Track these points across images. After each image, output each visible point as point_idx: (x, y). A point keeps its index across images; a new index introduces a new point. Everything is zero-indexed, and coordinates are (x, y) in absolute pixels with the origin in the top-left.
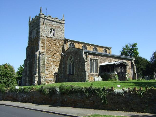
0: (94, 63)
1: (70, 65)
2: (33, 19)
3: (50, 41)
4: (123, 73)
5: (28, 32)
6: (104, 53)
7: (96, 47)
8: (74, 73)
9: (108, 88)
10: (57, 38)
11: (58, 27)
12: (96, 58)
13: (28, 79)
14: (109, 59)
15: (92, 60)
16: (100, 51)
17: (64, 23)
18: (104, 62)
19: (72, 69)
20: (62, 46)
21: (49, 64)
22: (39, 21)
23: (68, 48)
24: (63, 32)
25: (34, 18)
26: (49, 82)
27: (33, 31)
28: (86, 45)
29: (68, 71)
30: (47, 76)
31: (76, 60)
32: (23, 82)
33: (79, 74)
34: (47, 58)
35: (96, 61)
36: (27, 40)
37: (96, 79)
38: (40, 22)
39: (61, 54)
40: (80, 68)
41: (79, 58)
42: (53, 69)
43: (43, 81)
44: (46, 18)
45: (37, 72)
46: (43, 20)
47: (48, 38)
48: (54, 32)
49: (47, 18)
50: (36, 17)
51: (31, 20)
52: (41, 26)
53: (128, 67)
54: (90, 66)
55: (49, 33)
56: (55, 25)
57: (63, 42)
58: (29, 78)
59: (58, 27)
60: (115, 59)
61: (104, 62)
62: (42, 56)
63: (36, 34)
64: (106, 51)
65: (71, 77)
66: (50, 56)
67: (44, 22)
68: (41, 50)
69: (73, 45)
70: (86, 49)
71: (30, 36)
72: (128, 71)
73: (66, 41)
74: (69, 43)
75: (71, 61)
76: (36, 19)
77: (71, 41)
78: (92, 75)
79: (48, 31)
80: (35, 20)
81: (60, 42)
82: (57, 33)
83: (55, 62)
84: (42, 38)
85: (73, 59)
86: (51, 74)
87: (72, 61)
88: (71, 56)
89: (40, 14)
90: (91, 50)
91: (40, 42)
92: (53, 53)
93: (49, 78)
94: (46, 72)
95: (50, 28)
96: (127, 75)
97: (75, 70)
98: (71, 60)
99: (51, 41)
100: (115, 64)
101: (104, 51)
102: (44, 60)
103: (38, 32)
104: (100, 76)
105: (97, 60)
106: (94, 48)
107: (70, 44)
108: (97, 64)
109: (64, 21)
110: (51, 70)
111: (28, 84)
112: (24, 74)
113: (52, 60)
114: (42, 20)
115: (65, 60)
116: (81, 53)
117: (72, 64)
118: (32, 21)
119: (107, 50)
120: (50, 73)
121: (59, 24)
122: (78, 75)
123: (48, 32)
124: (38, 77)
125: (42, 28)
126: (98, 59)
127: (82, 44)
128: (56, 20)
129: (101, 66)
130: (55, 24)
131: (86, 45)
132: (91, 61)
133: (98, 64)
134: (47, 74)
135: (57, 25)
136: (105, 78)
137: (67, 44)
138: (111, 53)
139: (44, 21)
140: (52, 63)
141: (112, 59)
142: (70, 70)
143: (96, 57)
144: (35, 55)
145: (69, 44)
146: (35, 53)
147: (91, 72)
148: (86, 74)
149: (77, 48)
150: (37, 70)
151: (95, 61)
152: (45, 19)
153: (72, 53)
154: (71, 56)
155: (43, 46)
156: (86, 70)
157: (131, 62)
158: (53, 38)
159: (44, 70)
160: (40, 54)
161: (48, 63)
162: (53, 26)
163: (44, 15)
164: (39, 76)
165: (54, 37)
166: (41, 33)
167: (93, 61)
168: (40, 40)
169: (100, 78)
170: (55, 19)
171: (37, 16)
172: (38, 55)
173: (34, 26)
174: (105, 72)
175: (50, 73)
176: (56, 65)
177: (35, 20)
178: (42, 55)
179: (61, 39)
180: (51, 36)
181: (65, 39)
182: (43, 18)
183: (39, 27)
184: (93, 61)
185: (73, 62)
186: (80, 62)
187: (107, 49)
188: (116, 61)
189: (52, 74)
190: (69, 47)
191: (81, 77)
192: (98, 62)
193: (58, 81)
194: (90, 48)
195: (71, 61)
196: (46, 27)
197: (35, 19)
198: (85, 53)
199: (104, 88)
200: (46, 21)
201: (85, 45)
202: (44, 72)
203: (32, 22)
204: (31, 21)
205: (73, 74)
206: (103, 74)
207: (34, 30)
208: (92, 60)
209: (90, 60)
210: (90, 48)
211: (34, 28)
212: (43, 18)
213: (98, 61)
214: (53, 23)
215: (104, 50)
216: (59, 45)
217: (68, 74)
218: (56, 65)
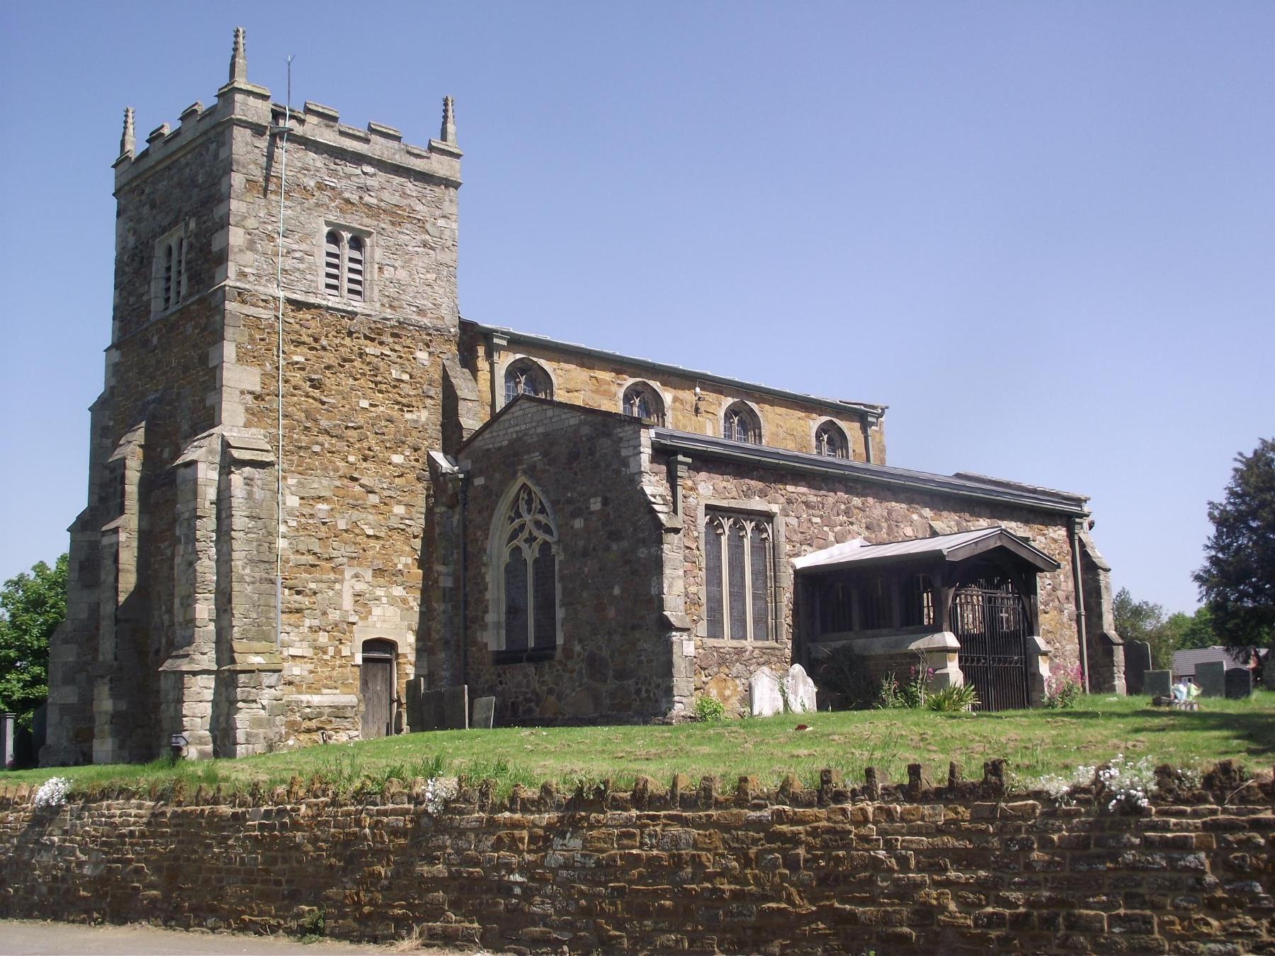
0: (747, 543)
1: (514, 569)
2: (155, 137)
3: (324, 342)
4: (1014, 635)
5: (114, 254)
6: (826, 456)
7: (746, 401)
8: (560, 641)
9: (952, 773)
10: (388, 313)
11: (397, 216)
12: (757, 504)
13: (105, 704)
14: (877, 509)
15: (727, 524)
16: (786, 434)
17: (457, 177)
18: (831, 537)
19: (537, 607)
20: (436, 392)
21: (310, 559)
22: (216, 155)
23: (493, 405)
24: (446, 257)
25: (167, 131)
26: (314, 724)
27: (159, 252)
28: (656, 385)
29: (497, 625)
30: (296, 670)
31: (574, 515)
32: (55, 735)
33: (605, 653)
34: (293, 501)
35: (758, 529)
36: (102, 331)
37: (766, 701)
38: (228, 167)
39: (432, 462)
40: (617, 591)
41: (605, 503)
42: (348, 603)
43: (257, 722)
44: (290, 124)
45: (206, 629)
46: (263, 143)
47: (305, 315)
48: (356, 255)
49: (298, 130)
50: (188, 115)
51: (135, 147)
52: (234, 205)
53: (1043, 582)
54: (703, 574)
55: (312, 269)
56: (367, 199)
57: (451, 352)
58: (115, 695)
59: (397, 216)
60: (927, 512)
61: (831, 537)
62: (249, 481)
63: (184, 279)
64: (835, 438)
65: (524, 677)
66: (321, 485)
67: (268, 167)
68: (234, 423)
69: (541, 380)
70: (661, 413)
71: (130, 294)
72: (1045, 621)
73: (473, 340)
74: (505, 360)
75: (522, 527)
76: (188, 136)
77: (516, 342)
78: (723, 662)
79: (304, 247)
80: (174, 146)
81: (419, 355)
82: (388, 273)
83: (372, 543)
84: (248, 310)
85: (542, 510)
86: (331, 651)
87: (530, 526)
88: (522, 479)
89: (227, 95)
90: (703, 427)
91: (229, 350)
92: (351, 459)
93: (317, 691)
95: (328, 223)
96: (1045, 654)
97: (560, 613)
98: (527, 518)
99: (338, 339)
100: (937, 556)
101: (818, 436)
102: (262, 519)
103: (208, 259)
104: (798, 669)
105: (769, 517)
106: (731, 412)
107: (513, 372)
108: (767, 552)
109: (458, 156)
110: (334, 615)
111: (103, 745)
112: (66, 655)
113: (342, 525)
114: (244, 145)
115: (465, 525)
116: (624, 453)
117: (530, 554)
118: (145, 154)
119: (851, 429)
120: (323, 638)
121: (411, 187)
122: (594, 664)
123: (301, 260)
124: (210, 681)
125: (251, 223)
126: (775, 508)
127: (619, 372)
128: (379, 148)
129: (807, 578)
130: (370, 182)
131: (656, 385)
132: (713, 526)
133: (784, 560)
134: (293, 651)
135: (385, 195)
136: (845, 687)
137: (484, 375)
138: (883, 461)
139: (270, 157)
140: (340, 551)
141: (899, 507)
142: (514, 611)
143: (763, 494)
144: (182, 471)
145: (501, 371)
146: (178, 453)
147: (715, 629)
148: (669, 646)
149: (580, 403)
150: (204, 609)
151: (749, 526)
152: (273, 136)
153: (536, 456)
154: (522, 479)
155: (257, 389)
156: (674, 609)
157: (1071, 535)
158: (352, 315)
159: (264, 606)
160: (228, 464)
161: (302, 548)
162: (348, 201)
163: (265, 98)
164: (227, 681)
165: (358, 305)
166: (243, 265)
167: (738, 528)
168: (229, 332)
169: (804, 692)
170: (367, 141)
171: (201, 109)
172: (214, 475)
173: (173, 212)
174: (852, 630)
175: (323, 638)
176: (379, 572)
177: (174, 146)
178: (247, 470)
179: (425, 321)
180: (332, 302)
181: (466, 326)
182: (258, 130)
183: (219, 211)
184: (738, 528)
185: (541, 536)
186: (614, 535)
187: (842, 417)
188: (938, 525)
190: (501, 403)
191: (621, 675)
192: (783, 539)
194: (697, 410)
195: (522, 527)
196: (285, 211)
197: (177, 134)
198: (665, 454)
199: (826, 776)
200: (284, 152)
201: (648, 377)
202: (263, 633)
203: (181, 141)
204: (133, 156)
205: (543, 654)
206: (823, 650)
207: (174, 242)
208: (727, 524)
209: (702, 520)
210: (697, 410)
211: (175, 223)
212: (258, 130)
213: (783, 529)
214: (350, 178)
215: (822, 430)
216: (406, 377)
217: (492, 647)
218: (379, 572)
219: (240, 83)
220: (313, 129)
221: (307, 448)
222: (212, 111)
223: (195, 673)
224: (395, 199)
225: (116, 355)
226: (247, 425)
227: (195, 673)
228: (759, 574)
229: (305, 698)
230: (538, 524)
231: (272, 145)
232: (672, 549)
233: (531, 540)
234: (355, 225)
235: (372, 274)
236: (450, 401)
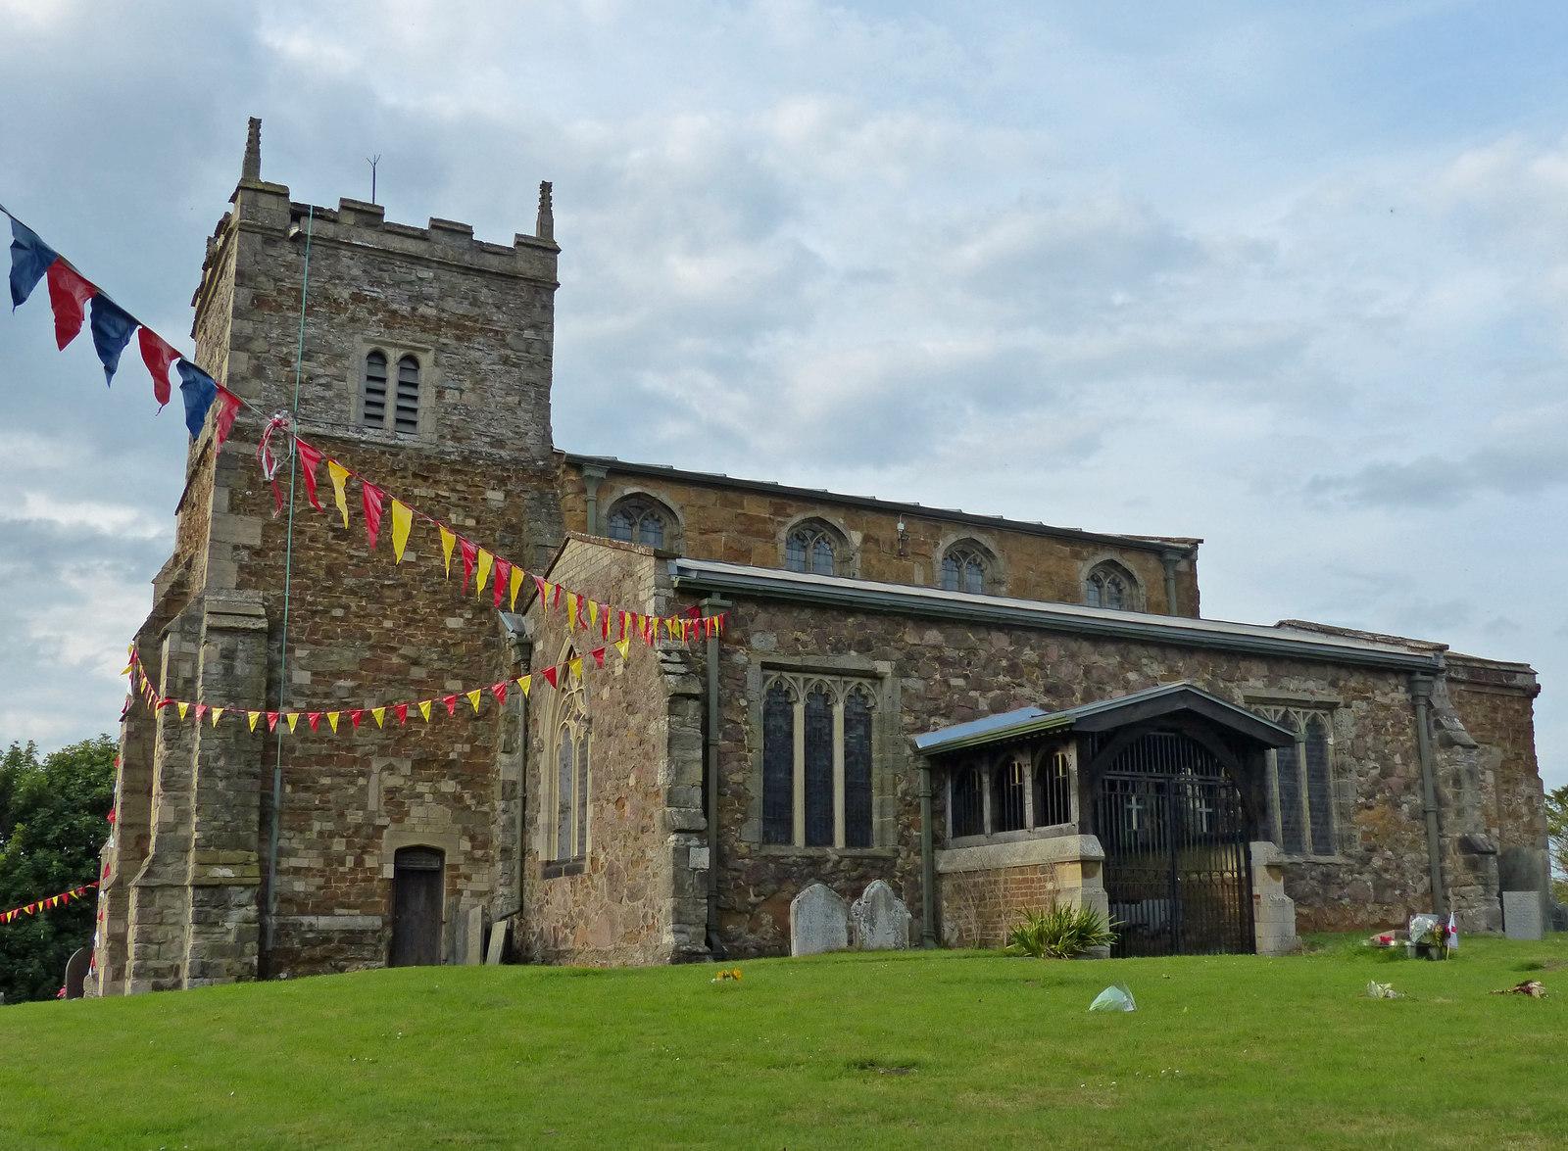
12: (852, 660)
56: (422, 309)
66: (343, 656)
81: (490, 494)
94: (283, 843)
110: (355, 817)
120: (338, 845)
123: (327, 386)
126: (883, 667)
134: (294, 862)
143: (864, 647)
145: (368, 288)
155: (257, 542)
189: (359, 862)
193: (1312, 780)
218: (420, 764)
235: (426, 400)
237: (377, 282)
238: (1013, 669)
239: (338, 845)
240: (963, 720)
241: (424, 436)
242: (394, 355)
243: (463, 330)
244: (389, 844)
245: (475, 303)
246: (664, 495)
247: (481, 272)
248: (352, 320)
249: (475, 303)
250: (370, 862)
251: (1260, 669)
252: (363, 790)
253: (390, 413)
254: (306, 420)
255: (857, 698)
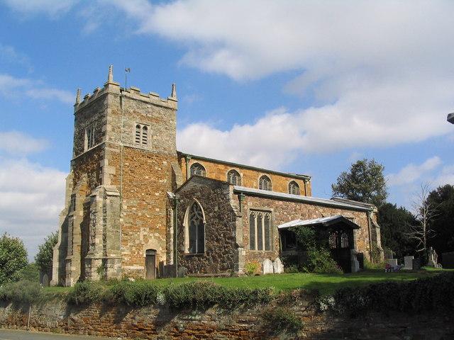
12: (266, 208)
17: (176, 108)
25: (90, 96)
42: (142, 238)
46: (118, 99)
48: (145, 132)
49: (128, 95)
51: (81, 101)
53: (357, 233)
56: (148, 115)
66: (134, 202)
68: (107, 183)
73: (181, 156)
77: (194, 158)
81: (164, 162)
91: (106, 162)
110: (137, 242)
119: (300, 182)
120: (134, 249)
121: (162, 111)
123: (128, 134)
126: (272, 210)
134: (125, 253)
140: (139, 222)
143: (268, 205)
145: (189, 167)
156: (239, 240)
168: (106, 156)
169: (280, 268)
173: (90, 113)
181: (179, 153)
189: (138, 253)
190: (189, 177)
212: (116, 95)
218: (151, 229)
219: (111, 81)
220: (132, 94)
221: (129, 191)
222: (103, 90)
223: (95, 259)
224: (157, 115)
225: (74, 163)
226: (112, 184)
227: (95, 259)
228: (267, 230)
229: (86, 135)
230: (199, 214)
231: (121, 100)
232: (239, 222)
233: (197, 219)
234: (144, 123)
235: (149, 138)
236: (174, 176)
237: (139, 108)
238: (295, 210)
239: (134, 249)
240: (286, 222)
241: (149, 148)
242: (142, 126)
243: (157, 120)
244: (145, 249)
245: (160, 114)
246: (202, 163)
247: (161, 106)
248: (134, 117)
249: (160, 114)
250: (141, 253)
251: (340, 210)
252: (139, 235)
253: (142, 141)
254: (124, 142)
255: (266, 217)
